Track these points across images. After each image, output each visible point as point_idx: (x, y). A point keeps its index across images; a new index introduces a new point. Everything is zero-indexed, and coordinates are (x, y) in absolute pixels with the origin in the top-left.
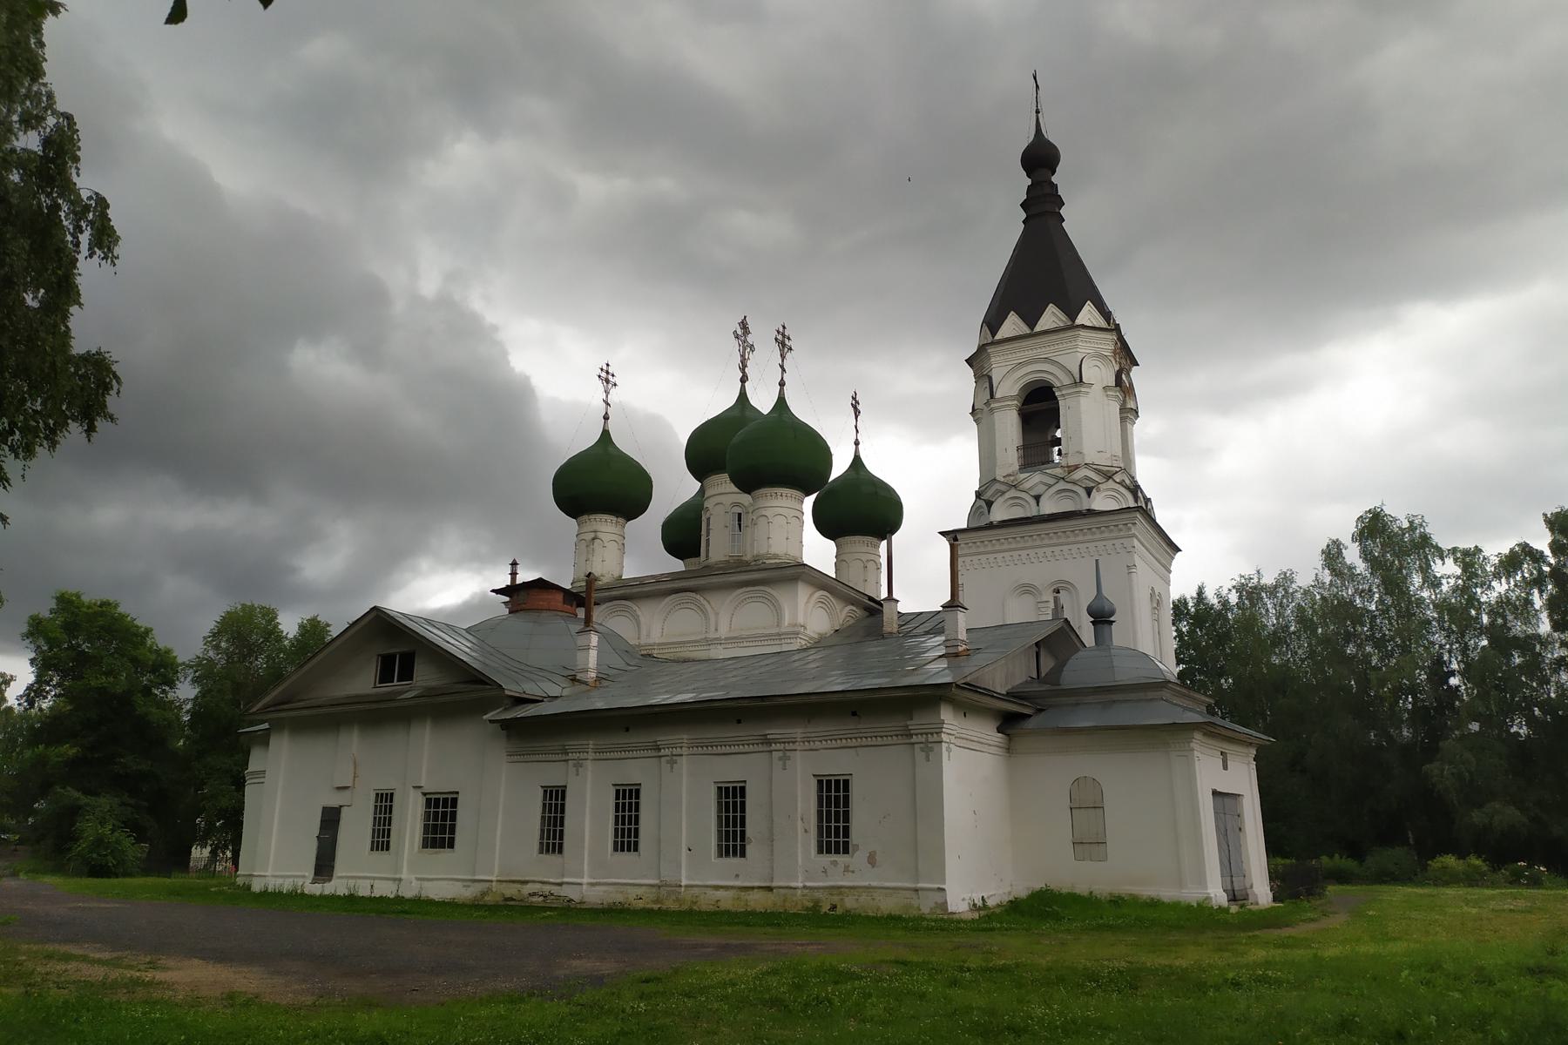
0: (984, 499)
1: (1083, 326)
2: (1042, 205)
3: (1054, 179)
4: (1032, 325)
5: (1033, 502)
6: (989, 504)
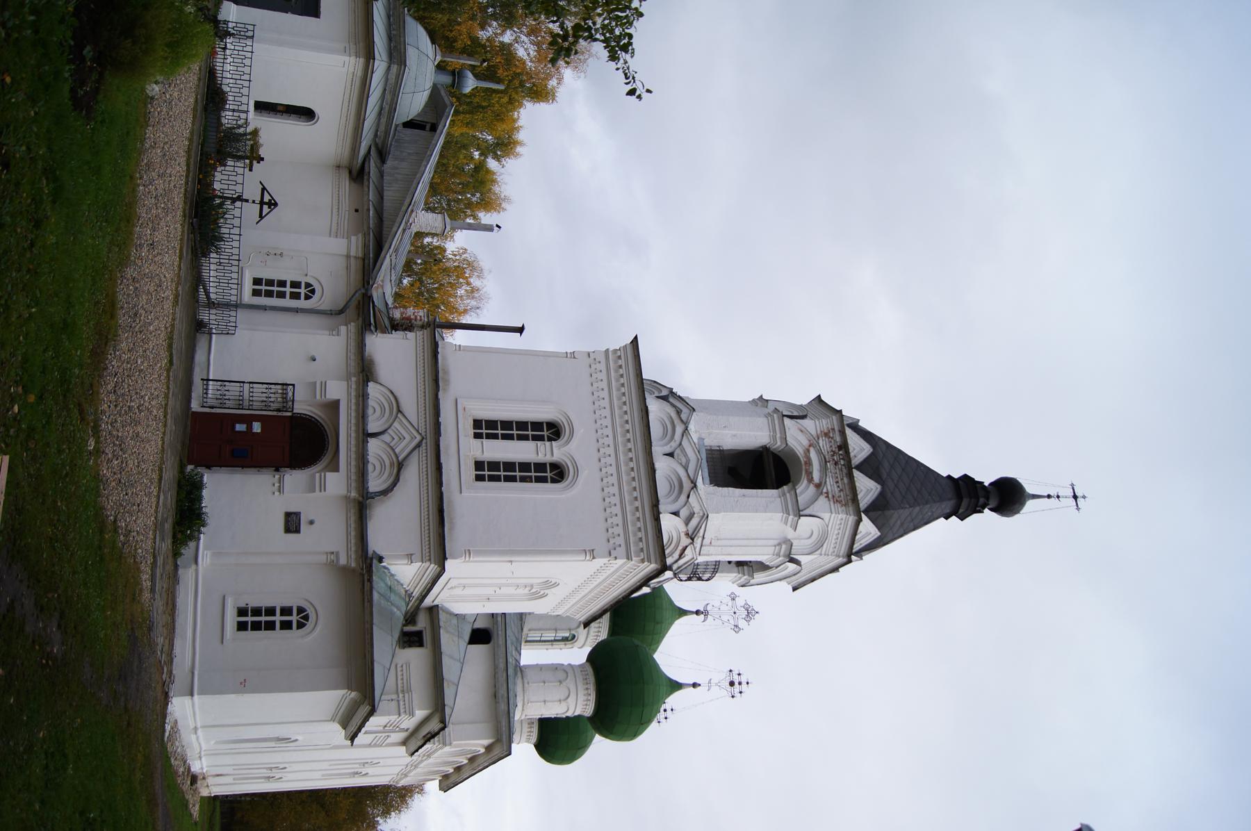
0: (669, 396)
1: (860, 520)
2: (967, 496)
3: (986, 510)
4: (860, 467)
5: (668, 449)
6: (664, 398)
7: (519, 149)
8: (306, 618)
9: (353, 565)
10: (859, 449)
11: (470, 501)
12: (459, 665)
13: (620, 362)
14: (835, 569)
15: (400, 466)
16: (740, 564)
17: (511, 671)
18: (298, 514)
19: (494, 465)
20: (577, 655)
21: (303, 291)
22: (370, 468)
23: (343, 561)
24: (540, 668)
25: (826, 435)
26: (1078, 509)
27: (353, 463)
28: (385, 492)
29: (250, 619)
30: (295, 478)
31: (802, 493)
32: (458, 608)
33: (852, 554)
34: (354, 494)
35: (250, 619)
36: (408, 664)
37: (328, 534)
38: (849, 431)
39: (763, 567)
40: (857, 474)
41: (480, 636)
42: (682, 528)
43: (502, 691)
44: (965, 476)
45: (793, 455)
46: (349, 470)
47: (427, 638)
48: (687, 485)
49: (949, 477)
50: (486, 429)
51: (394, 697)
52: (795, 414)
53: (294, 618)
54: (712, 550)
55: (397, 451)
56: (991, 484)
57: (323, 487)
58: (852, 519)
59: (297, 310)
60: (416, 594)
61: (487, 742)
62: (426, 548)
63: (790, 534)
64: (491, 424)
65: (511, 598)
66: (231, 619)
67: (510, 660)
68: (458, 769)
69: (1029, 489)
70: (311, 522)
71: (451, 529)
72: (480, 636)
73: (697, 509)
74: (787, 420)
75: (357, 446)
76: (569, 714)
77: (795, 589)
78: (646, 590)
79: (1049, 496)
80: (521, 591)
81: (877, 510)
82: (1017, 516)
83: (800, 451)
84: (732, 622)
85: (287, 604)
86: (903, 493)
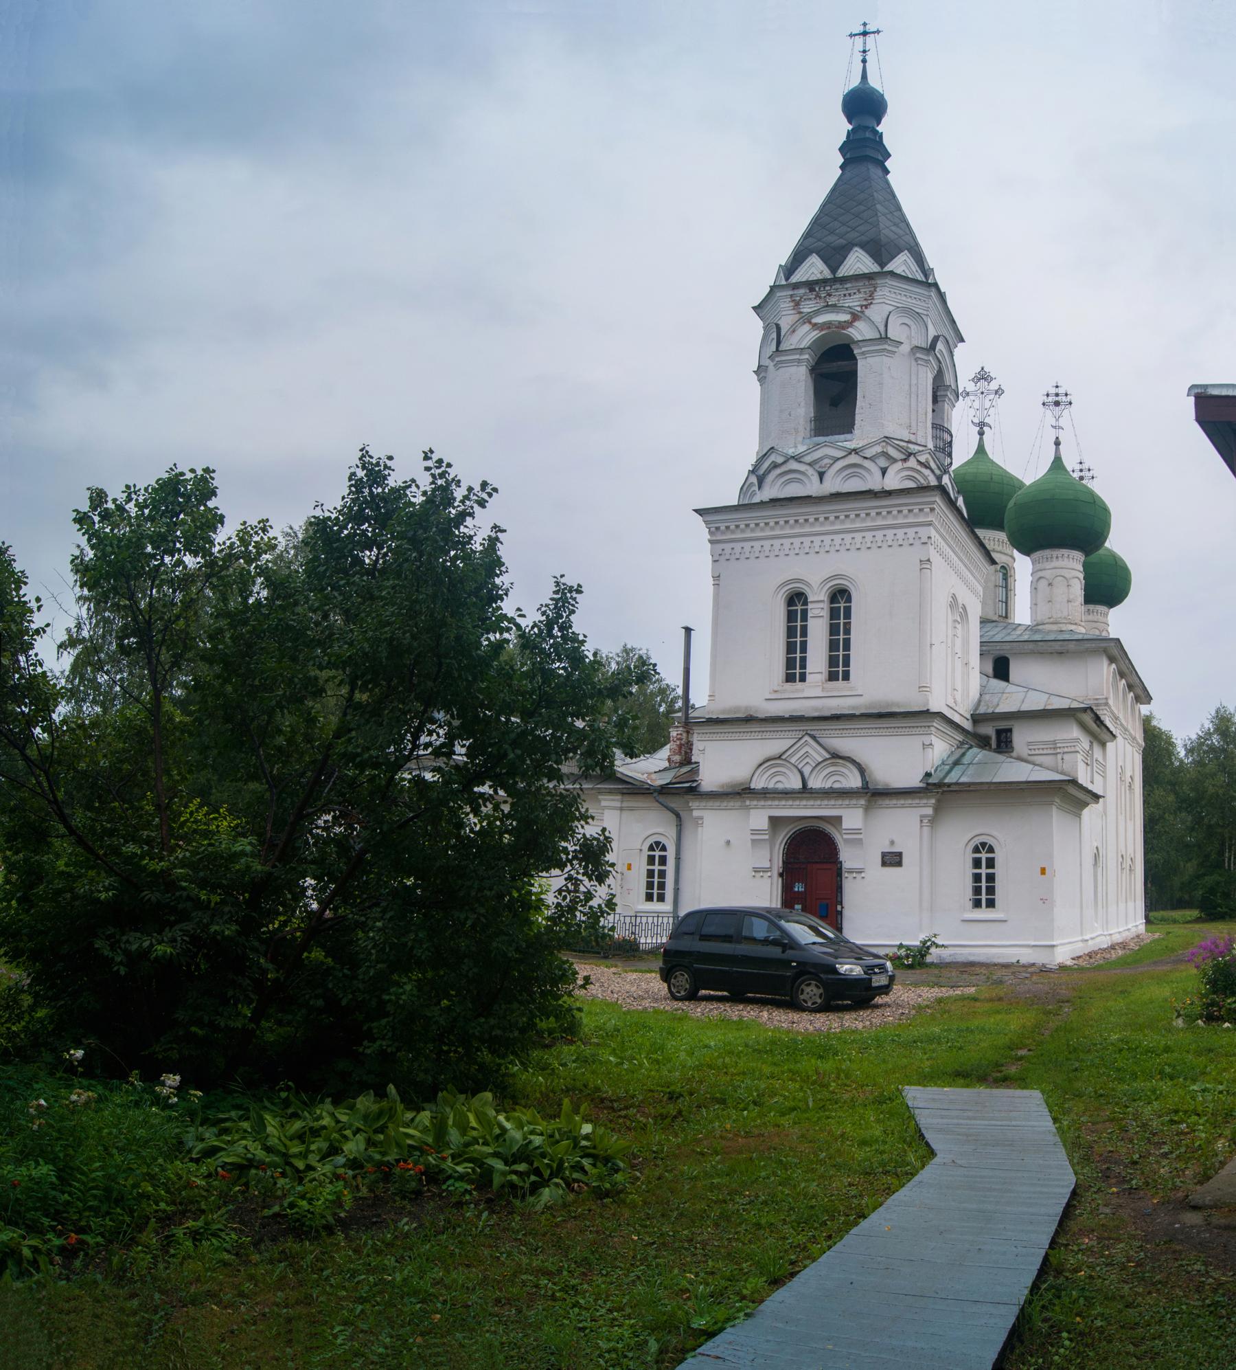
0: (759, 474)
2: (864, 150)
3: (879, 129)
4: (834, 270)
5: (816, 478)
7: (408, 473)
8: (983, 844)
9: (933, 801)
10: (814, 268)
11: (871, 684)
12: (1030, 692)
13: (723, 528)
14: (942, 297)
15: (835, 756)
16: (935, 400)
17: (1037, 637)
18: (884, 855)
19: (833, 661)
20: (1022, 565)
21: (657, 853)
22: (836, 786)
23: (930, 811)
24: (1034, 605)
25: (797, 304)
26: (878, 32)
27: (832, 802)
28: (862, 770)
29: (984, 897)
30: (848, 857)
31: (861, 333)
32: (974, 693)
33: (927, 282)
34: (862, 802)
35: (984, 897)
36: (1029, 743)
37: (901, 826)
38: (794, 279)
39: (939, 378)
40: (842, 272)
41: (1001, 669)
42: (899, 465)
43: (1057, 646)
44: (840, 149)
45: (816, 342)
46: (841, 807)
47: (1003, 725)
48: (854, 459)
49: (842, 167)
50: (794, 670)
51: (1059, 756)
52: (774, 335)
53: (984, 856)
54: (920, 433)
55: (820, 759)
56: (850, 122)
57: (857, 831)
58: (890, 281)
59: (678, 858)
60: (960, 738)
61: (1105, 662)
62: (918, 731)
63: (905, 348)
64: (790, 663)
65: (966, 642)
66: (984, 913)
67: (1025, 637)
68: (1130, 687)
69: (855, 82)
70: (892, 843)
71: (898, 705)
72: (1001, 669)
73: (878, 449)
74: (783, 347)
75: (815, 799)
76: (1081, 576)
77: (962, 340)
78: (960, 502)
79: (864, 61)
80: (959, 632)
81: (881, 251)
82: (886, 97)
83: (815, 334)
84: (991, 397)
85: (970, 863)
86: (858, 226)
